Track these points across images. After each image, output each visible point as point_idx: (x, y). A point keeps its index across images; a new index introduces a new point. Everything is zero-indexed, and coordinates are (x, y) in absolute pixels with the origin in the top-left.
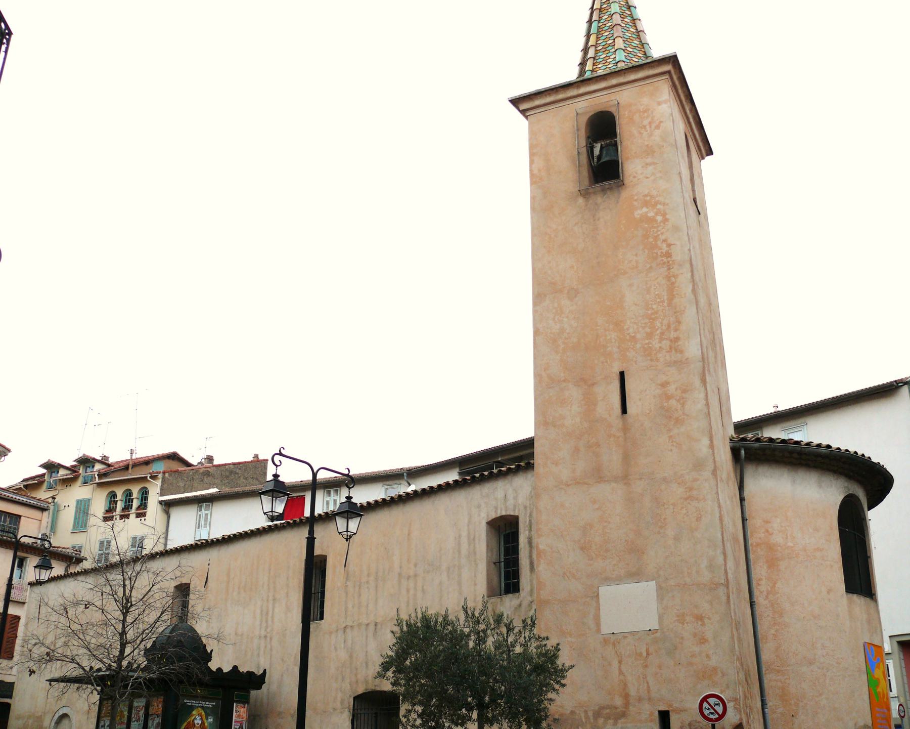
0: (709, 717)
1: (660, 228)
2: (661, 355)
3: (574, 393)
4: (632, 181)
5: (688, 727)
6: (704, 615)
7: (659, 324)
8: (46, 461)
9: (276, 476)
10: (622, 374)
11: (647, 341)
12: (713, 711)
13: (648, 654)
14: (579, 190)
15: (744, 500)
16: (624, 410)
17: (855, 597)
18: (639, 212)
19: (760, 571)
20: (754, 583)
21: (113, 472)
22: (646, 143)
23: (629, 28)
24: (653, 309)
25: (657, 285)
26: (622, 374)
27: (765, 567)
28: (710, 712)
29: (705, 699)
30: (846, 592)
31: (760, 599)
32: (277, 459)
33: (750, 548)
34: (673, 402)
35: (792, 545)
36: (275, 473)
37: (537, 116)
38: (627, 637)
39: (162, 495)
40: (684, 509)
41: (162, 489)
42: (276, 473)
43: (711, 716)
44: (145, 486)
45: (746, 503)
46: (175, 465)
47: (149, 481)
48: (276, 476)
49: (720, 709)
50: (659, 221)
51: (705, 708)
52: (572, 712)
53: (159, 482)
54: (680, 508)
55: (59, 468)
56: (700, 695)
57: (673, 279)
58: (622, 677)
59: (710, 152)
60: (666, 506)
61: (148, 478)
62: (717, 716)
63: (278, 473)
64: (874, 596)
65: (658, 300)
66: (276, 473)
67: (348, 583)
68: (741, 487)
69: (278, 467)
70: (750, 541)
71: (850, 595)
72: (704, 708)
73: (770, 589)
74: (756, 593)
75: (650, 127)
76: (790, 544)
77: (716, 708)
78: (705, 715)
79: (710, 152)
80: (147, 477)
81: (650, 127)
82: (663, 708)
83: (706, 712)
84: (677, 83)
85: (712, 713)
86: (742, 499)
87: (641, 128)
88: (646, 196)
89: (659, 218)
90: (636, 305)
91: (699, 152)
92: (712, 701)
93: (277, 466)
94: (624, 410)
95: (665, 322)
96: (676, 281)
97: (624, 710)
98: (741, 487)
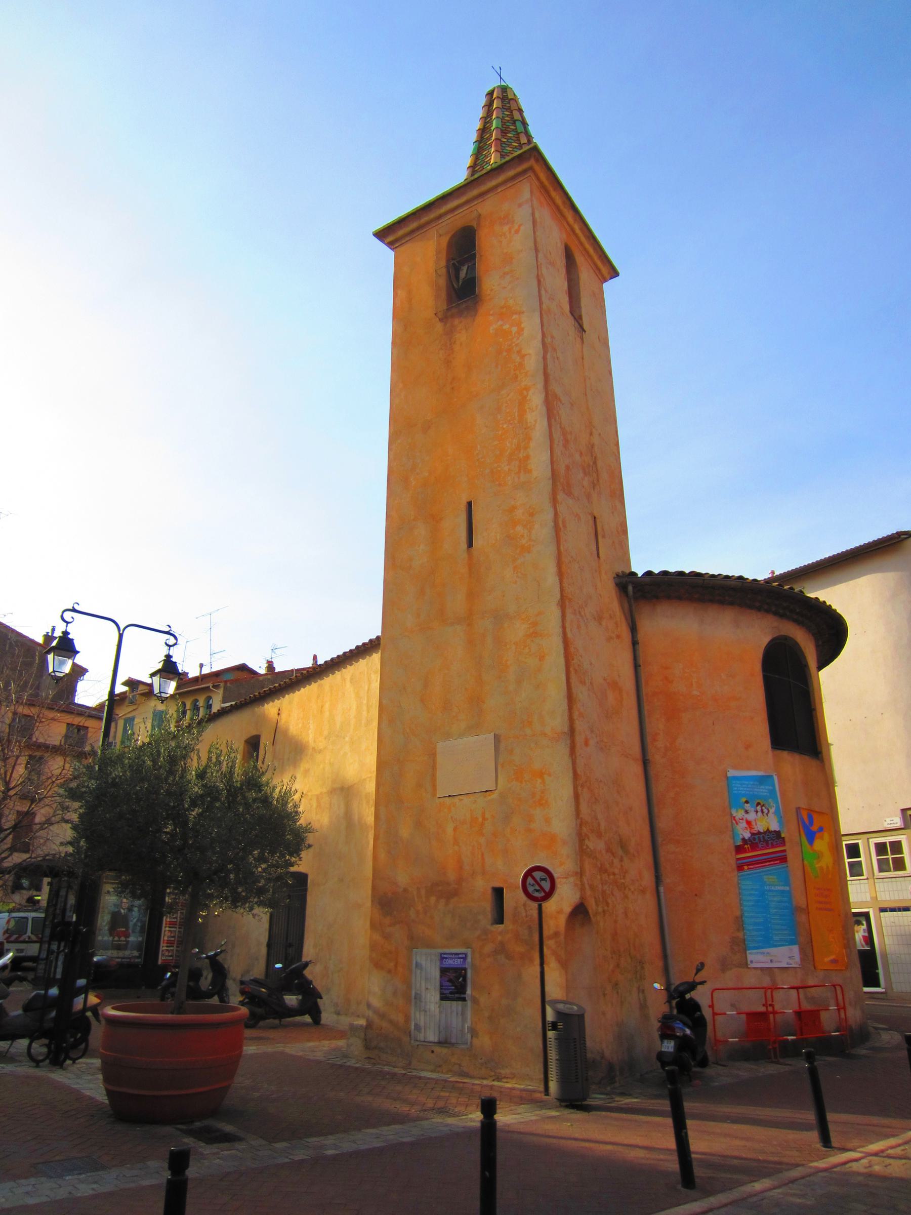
0: (534, 895)
1: (515, 340)
2: (509, 478)
3: (421, 530)
4: (489, 295)
5: (522, 907)
6: (544, 771)
7: (508, 445)
8: (127, 678)
9: (66, 633)
10: (470, 504)
11: (496, 465)
12: (537, 888)
13: (484, 819)
14: (435, 314)
15: (638, 643)
16: (470, 544)
17: (785, 755)
18: (494, 326)
19: (657, 724)
20: (649, 739)
21: (184, 684)
22: (505, 251)
23: (504, 147)
24: (504, 429)
25: (509, 402)
26: (470, 504)
27: (663, 720)
28: (535, 890)
29: (529, 873)
30: (772, 748)
31: (657, 759)
32: (68, 616)
33: (645, 698)
34: (519, 528)
35: (698, 694)
36: (64, 630)
37: (398, 249)
38: (462, 800)
39: (224, 702)
40: (527, 648)
41: (224, 697)
42: (66, 630)
43: (537, 894)
44: (210, 695)
45: (640, 648)
46: (245, 675)
47: (211, 690)
48: (66, 633)
49: (546, 885)
50: (513, 333)
51: (530, 884)
52: (405, 890)
53: (221, 691)
54: (523, 647)
55: (138, 685)
56: (526, 865)
57: (525, 393)
58: (456, 848)
59: (615, 273)
60: (508, 647)
61: (211, 687)
62: (542, 894)
63: (68, 631)
64: (820, 755)
65: (509, 418)
66: (66, 630)
67: (274, 761)
68: (633, 629)
69: (69, 624)
70: (644, 690)
71: (778, 752)
72: (528, 883)
73: (668, 745)
74: (651, 749)
75: (510, 232)
76: (695, 693)
77: (543, 884)
78: (529, 893)
79: (615, 273)
80: (209, 686)
81: (510, 232)
82: (498, 885)
83: (530, 889)
84: (546, 183)
85: (537, 891)
86: (635, 643)
87: (501, 236)
88: (502, 308)
89: (514, 329)
90: (487, 427)
91: (597, 272)
92: (538, 875)
93: (67, 623)
94: (470, 544)
95: (515, 441)
96: (528, 395)
97: (456, 886)
98: (633, 629)
